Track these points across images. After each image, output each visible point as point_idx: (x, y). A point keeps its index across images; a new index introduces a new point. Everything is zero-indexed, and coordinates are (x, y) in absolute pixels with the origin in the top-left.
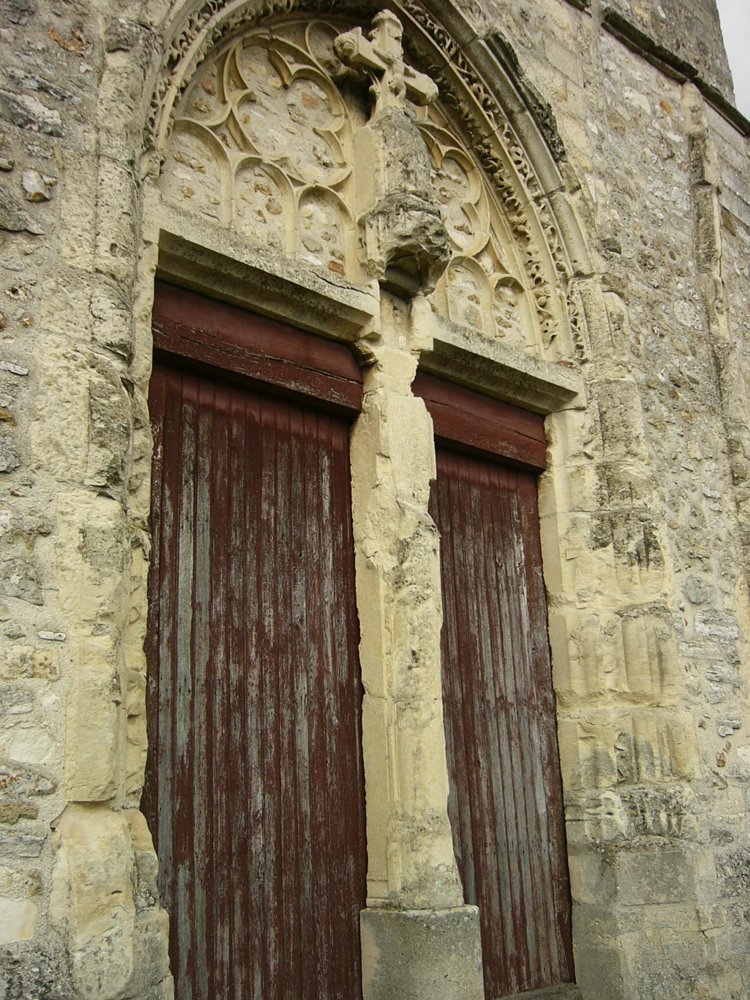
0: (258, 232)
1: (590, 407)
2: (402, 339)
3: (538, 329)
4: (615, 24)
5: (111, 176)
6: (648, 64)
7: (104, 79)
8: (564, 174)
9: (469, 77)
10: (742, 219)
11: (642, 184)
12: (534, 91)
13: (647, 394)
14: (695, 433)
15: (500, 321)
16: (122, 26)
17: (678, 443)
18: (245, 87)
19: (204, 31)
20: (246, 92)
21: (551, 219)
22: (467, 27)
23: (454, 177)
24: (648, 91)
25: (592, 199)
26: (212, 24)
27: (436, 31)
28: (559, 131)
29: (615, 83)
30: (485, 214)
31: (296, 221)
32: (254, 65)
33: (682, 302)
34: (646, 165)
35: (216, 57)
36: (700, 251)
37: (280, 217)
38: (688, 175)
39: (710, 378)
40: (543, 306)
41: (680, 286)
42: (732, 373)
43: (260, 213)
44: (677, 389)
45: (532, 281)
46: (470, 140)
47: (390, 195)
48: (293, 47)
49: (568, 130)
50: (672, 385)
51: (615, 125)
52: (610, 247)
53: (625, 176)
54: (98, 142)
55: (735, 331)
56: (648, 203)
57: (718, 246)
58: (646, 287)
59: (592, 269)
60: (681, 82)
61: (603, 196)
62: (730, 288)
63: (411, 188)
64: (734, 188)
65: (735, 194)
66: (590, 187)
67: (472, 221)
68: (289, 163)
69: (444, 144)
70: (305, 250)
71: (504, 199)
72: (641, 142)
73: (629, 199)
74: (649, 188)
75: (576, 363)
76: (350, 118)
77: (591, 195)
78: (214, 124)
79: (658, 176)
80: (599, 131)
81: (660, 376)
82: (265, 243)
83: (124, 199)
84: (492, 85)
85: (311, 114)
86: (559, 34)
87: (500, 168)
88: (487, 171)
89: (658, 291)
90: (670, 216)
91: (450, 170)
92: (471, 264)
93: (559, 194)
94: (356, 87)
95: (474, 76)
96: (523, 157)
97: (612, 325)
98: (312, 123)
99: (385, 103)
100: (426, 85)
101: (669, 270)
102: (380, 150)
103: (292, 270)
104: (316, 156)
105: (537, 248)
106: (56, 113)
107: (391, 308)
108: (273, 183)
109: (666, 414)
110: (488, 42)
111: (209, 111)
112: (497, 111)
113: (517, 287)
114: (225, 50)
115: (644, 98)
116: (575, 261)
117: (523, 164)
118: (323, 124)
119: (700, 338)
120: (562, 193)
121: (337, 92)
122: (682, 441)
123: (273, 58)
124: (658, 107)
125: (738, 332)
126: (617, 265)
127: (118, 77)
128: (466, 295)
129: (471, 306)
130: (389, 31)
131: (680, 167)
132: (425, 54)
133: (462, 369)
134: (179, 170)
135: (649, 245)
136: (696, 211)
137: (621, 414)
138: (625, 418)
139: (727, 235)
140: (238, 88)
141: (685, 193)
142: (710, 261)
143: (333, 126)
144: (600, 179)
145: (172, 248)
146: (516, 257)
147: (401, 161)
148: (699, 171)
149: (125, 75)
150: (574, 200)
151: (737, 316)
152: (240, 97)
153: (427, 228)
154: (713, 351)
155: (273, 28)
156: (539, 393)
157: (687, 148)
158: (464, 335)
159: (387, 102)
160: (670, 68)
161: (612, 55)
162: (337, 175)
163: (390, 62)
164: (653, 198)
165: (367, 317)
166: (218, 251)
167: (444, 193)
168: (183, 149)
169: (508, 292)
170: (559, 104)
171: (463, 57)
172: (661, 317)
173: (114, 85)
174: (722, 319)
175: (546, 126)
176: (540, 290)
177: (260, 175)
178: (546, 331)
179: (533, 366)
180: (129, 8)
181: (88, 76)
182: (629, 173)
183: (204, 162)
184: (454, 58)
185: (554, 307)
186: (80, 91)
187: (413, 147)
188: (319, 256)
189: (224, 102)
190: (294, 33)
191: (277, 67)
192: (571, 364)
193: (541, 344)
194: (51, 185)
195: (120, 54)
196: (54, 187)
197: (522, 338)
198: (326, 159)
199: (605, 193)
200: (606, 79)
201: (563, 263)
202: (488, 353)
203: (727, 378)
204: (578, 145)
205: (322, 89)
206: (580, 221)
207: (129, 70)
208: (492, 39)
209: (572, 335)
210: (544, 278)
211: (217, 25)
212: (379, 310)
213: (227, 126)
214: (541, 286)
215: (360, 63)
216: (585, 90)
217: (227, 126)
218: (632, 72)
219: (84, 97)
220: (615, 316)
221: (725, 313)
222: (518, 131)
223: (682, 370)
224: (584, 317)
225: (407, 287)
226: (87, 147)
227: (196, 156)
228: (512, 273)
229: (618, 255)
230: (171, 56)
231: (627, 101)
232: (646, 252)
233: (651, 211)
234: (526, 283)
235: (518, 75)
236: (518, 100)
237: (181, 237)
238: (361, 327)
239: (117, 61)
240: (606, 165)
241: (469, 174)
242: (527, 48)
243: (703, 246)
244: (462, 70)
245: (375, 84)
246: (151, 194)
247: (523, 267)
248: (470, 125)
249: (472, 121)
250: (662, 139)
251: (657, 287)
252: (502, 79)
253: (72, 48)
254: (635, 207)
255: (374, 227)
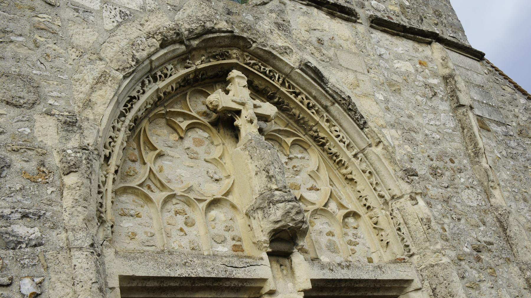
0: (182, 243)
1: (424, 286)
2: (290, 285)
3: (376, 239)
4: (379, 24)
5: (80, 260)
6: (405, 40)
7: (65, 194)
8: (369, 136)
9: (294, 93)
10: (492, 118)
11: (420, 120)
12: (337, 91)
13: (460, 266)
14: (501, 282)
15: (350, 243)
16: (69, 155)
17: (491, 294)
18: (155, 149)
19: (123, 129)
20: (157, 152)
21: (367, 166)
22: (287, 64)
23: (299, 156)
24: (410, 58)
25: (391, 145)
26: (127, 122)
27: (268, 72)
28: (359, 109)
29: (387, 61)
30: (324, 174)
31: (206, 225)
32: (159, 131)
33: (466, 191)
34: (420, 107)
35: (134, 137)
36: (470, 151)
37: (195, 227)
38: (448, 103)
39: (500, 237)
40: (376, 224)
41: (462, 180)
42: (514, 229)
43: (181, 230)
44: (479, 254)
45: (365, 208)
46: (305, 130)
47: (262, 194)
48: (181, 112)
49: (364, 106)
50: (475, 253)
51: (393, 89)
52: (410, 174)
53: (408, 120)
54: (67, 239)
55: (508, 198)
56: (427, 132)
57: (481, 145)
58: (440, 190)
59: (402, 192)
60: (430, 43)
61: (397, 139)
62: (496, 169)
63: (274, 187)
64: (481, 99)
65: (483, 103)
66: (387, 137)
67: (317, 181)
68: (194, 188)
69: (288, 137)
70: (215, 244)
71: (335, 161)
72: (413, 93)
73: (414, 134)
74: (425, 121)
75: (407, 258)
76: (226, 144)
77: (389, 142)
78: (141, 182)
79: (429, 112)
80: (384, 97)
81: (465, 249)
82: (189, 250)
83: (92, 273)
84: (310, 93)
85: (201, 150)
86: (344, 44)
87: (327, 143)
88: (320, 146)
89: (449, 189)
90: (444, 135)
91: (296, 153)
92: (323, 211)
93: (369, 149)
94: (225, 122)
95: (297, 91)
96: (339, 130)
97: (424, 227)
98: (203, 156)
99: (246, 131)
100: (269, 109)
101: (452, 172)
102: (249, 164)
103: (209, 269)
104: (210, 176)
105: (363, 187)
106: (36, 229)
107: (279, 266)
108: (186, 206)
109: (477, 276)
110: (302, 69)
111: (136, 173)
112: (317, 109)
113: (355, 215)
114: (139, 129)
115: (408, 63)
116: (390, 189)
117: (341, 137)
118: (210, 153)
119: (485, 211)
120: (370, 148)
121: (214, 130)
122: (493, 291)
123: (170, 123)
124: (418, 66)
125: (511, 197)
126: (417, 185)
127: (74, 191)
128: (325, 233)
129: (330, 240)
130: (239, 84)
131: (442, 99)
132: (264, 87)
133: (333, 290)
134: (124, 221)
135: (435, 160)
136: (460, 125)
137: (446, 287)
138: (450, 290)
139: (485, 133)
140: (151, 150)
141: (450, 116)
142: (478, 156)
143: (216, 153)
144: (392, 128)
145: (129, 283)
146: (351, 196)
147: (264, 170)
148: (455, 99)
149: (78, 188)
150: (379, 150)
151: (506, 187)
152: (154, 156)
153: (290, 212)
154: (497, 217)
155: (166, 104)
156: (388, 287)
157: (443, 85)
158: (330, 269)
159: (248, 129)
160: (420, 37)
161: (381, 43)
162: (226, 184)
163: (243, 104)
164: (429, 127)
165: (264, 280)
166: (159, 276)
167: (295, 169)
168: (124, 206)
169: (351, 220)
170: (355, 91)
171: (288, 82)
172: (455, 207)
173: (72, 197)
174: (496, 193)
175: (350, 110)
176: (371, 213)
177: (177, 203)
178: (382, 240)
179: (379, 272)
180: (72, 139)
181: (53, 195)
182: (410, 117)
183: (139, 209)
184: (283, 84)
185: (383, 224)
186: (50, 207)
187: (270, 159)
188: (225, 245)
189: (145, 163)
190: (180, 101)
191: (173, 127)
192: (404, 259)
193: (381, 249)
194: (41, 283)
195: (72, 174)
196: (43, 284)
197: (367, 249)
198: (216, 177)
199: (397, 136)
200: (381, 61)
201: (382, 193)
202: (348, 275)
203: (512, 234)
204: (373, 113)
205: (204, 131)
206: (386, 163)
207: (79, 184)
208: (304, 67)
209: (399, 239)
210: (372, 205)
211: (130, 121)
212: (270, 273)
213: (149, 179)
214: (372, 210)
215: (225, 110)
216: (369, 74)
217: (149, 179)
218: (396, 49)
219: (53, 210)
220: (425, 220)
221: (498, 187)
222: (333, 117)
223: (479, 238)
224: (404, 225)
225: (286, 250)
226: (61, 245)
227: (133, 207)
228: (352, 208)
229: (416, 178)
230: (105, 156)
231: (397, 69)
232: (434, 165)
233: (430, 136)
234: (361, 211)
235: (325, 84)
236: (329, 99)
237: (133, 275)
238: (261, 288)
239: (71, 180)
240: (394, 118)
241: (309, 151)
242: (327, 62)
243: (470, 147)
244: (290, 90)
245: (237, 121)
246: (109, 253)
247: (357, 200)
248: (302, 122)
249: (303, 118)
250: (426, 85)
251: (448, 187)
252: (316, 89)
253: (40, 180)
254: (419, 137)
255: (257, 218)
